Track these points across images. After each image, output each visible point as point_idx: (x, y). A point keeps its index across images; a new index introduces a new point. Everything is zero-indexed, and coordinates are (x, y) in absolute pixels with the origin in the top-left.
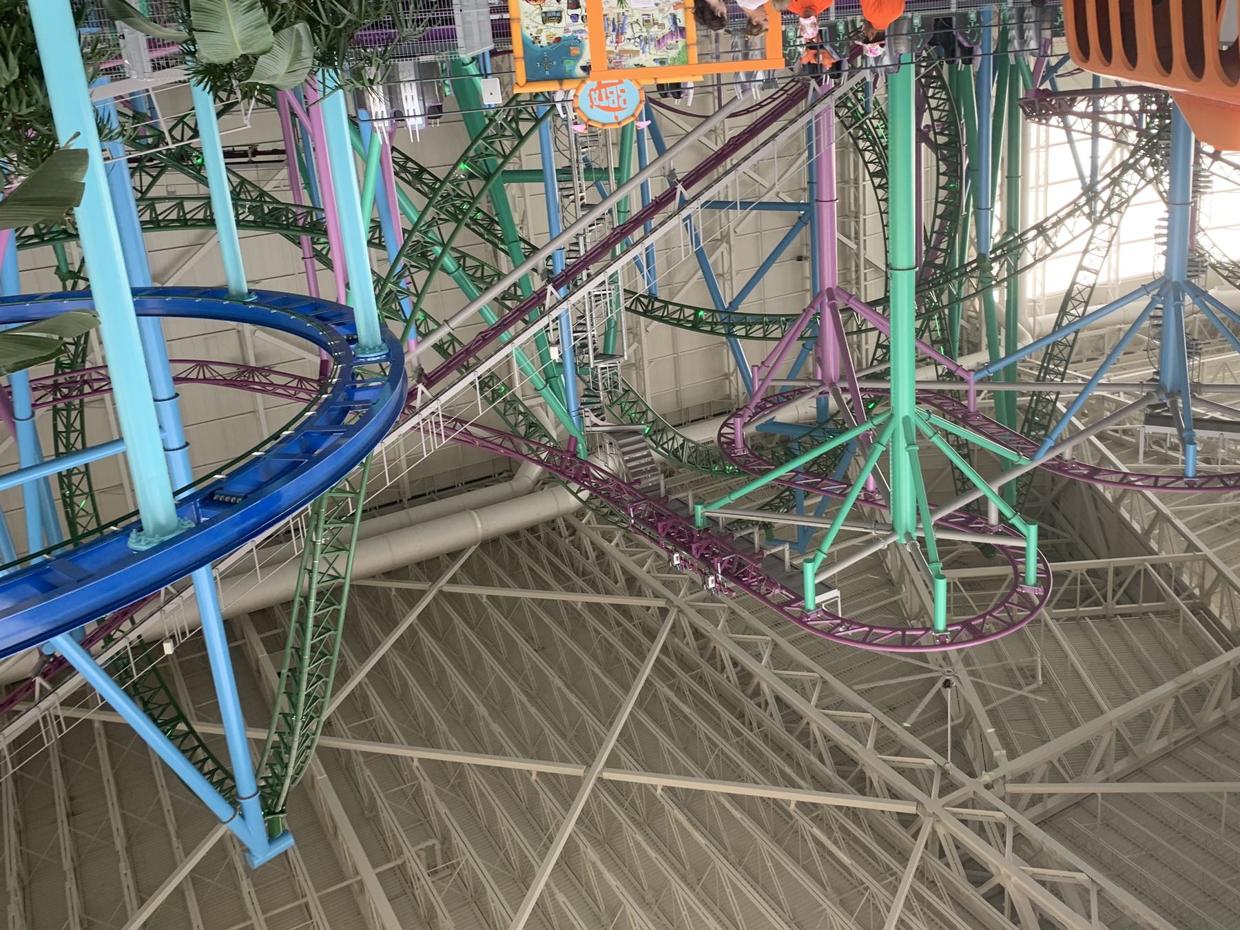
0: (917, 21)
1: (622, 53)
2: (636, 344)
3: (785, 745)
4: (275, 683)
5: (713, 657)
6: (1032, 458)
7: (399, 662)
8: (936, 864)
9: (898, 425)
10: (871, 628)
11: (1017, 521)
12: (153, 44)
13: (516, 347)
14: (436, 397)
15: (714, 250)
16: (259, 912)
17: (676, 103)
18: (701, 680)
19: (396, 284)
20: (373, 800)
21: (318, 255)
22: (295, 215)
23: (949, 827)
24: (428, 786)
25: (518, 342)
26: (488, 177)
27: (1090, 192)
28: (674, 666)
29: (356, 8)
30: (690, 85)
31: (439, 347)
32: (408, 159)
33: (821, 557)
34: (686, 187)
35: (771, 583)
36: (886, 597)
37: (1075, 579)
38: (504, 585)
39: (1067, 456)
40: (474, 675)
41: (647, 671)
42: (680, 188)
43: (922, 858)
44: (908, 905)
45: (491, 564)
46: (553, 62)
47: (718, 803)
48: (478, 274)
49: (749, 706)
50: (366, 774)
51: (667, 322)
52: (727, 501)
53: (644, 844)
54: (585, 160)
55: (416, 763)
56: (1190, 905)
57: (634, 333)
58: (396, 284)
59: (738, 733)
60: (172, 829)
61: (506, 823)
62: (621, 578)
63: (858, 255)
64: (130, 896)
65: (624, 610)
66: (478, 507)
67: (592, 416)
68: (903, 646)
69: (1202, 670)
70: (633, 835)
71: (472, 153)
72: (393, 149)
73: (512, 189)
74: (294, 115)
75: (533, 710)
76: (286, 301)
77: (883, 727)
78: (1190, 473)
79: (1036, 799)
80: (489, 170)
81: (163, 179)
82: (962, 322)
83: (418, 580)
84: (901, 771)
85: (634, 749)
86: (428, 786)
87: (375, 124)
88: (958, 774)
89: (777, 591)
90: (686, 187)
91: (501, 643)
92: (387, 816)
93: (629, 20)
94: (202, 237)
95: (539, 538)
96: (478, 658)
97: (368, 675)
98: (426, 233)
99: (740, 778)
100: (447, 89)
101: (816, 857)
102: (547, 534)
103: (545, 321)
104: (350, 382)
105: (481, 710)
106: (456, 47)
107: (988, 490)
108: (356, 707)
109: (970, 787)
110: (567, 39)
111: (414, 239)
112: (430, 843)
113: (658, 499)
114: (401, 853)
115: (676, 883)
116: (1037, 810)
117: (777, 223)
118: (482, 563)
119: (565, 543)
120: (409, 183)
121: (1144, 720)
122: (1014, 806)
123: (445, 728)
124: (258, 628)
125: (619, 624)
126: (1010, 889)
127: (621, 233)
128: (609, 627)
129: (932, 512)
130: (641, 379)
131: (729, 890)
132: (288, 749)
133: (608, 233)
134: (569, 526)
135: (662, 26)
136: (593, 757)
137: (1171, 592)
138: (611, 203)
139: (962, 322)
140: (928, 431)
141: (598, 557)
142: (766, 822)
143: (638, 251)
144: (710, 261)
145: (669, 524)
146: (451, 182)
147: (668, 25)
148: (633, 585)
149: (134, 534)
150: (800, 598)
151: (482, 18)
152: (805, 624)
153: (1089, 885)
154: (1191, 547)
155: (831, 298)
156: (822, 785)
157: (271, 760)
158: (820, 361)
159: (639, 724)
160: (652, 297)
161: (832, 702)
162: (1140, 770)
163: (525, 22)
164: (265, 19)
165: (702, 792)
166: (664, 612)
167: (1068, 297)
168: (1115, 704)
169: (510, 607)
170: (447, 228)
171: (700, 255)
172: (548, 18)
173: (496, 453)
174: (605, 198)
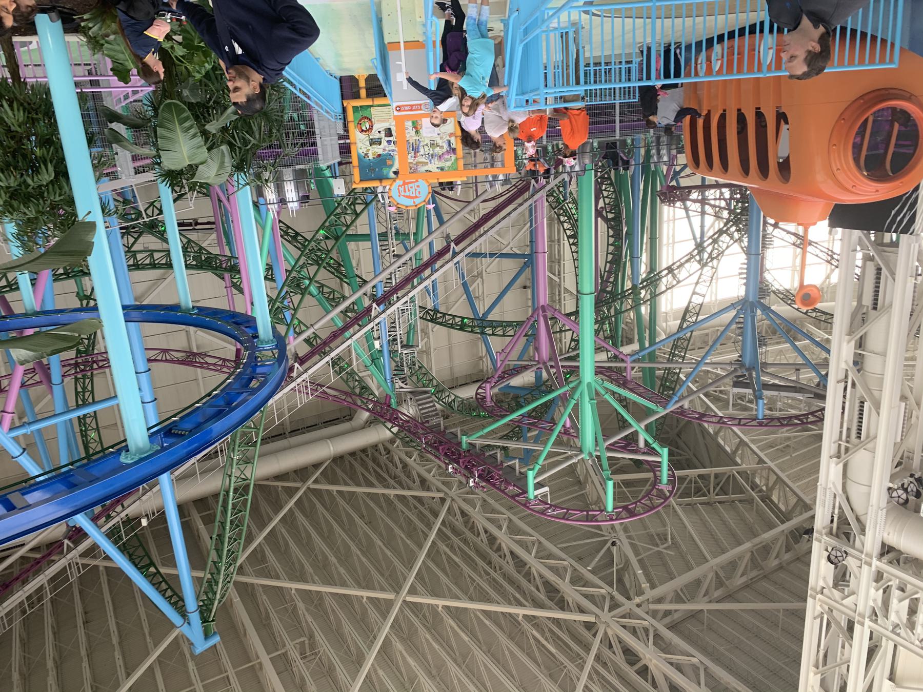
0: (595, 144)
1: (418, 163)
3: (516, 581)
4: (209, 543)
5: (473, 528)
6: (665, 408)
7: (283, 530)
8: (607, 652)
9: (584, 387)
10: (568, 510)
11: (655, 446)
12: (135, 158)
13: (354, 341)
14: (306, 371)
15: (473, 282)
17: (450, 194)
18: (465, 541)
19: (282, 302)
21: (235, 285)
23: (616, 630)
24: (301, 605)
25: (355, 338)
26: (337, 238)
27: (700, 247)
28: (449, 533)
29: (257, 136)
30: (459, 183)
31: (307, 341)
32: (289, 227)
33: (538, 467)
34: (456, 244)
35: (508, 483)
36: (576, 491)
37: (691, 480)
38: (346, 484)
40: (328, 538)
41: (433, 536)
42: (453, 245)
43: (599, 649)
44: (590, 677)
45: (338, 471)
47: (476, 615)
48: (331, 297)
49: (495, 557)
50: (263, 598)
51: (445, 326)
52: (481, 433)
53: (431, 640)
54: (395, 228)
55: (293, 591)
57: (425, 332)
58: (282, 302)
59: (487, 574)
60: (146, 631)
61: (348, 628)
62: (417, 480)
63: (560, 285)
64: (121, 672)
65: (419, 499)
66: (331, 437)
68: (587, 521)
69: (767, 536)
70: (424, 635)
71: (327, 224)
72: (280, 221)
73: (351, 246)
74: (220, 201)
75: (364, 559)
77: (575, 569)
79: (667, 613)
80: (337, 234)
81: (141, 240)
82: (623, 326)
83: (295, 481)
84: (586, 596)
85: (425, 583)
86: (301, 605)
87: (269, 206)
88: (620, 598)
89: (511, 488)
90: (456, 244)
91: (345, 519)
92: (277, 624)
93: (422, 144)
94: (164, 274)
95: (367, 456)
97: (265, 538)
98: (299, 272)
99: (489, 601)
101: (535, 648)
102: (373, 453)
105: (333, 559)
106: (317, 160)
107: (638, 427)
108: (257, 558)
109: (628, 606)
110: (385, 155)
112: (302, 639)
113: (439, 433)
114: (284, 646)
116: (668, 620)
117: (511, 267)
118: (333, 471)
119: (383, 459)
120: (289, 242)
121: (732, 565)
123: (311, 570)
125: (416, 508)
126: (651, 667)
127: (417, 272)
128: (410, 510)
129: (605, 440)
131: (482, 668)
132: (217, 583)
134: (386, 449)
136: (400, 588)
138: (411, 254)
139: (623, 326)
140: (602, 392)
141: (403, 468)
142: (506, 629)
143: (428, 283)
144: (471, 289)
147: (446, 146)
148: (424, 484)
149: (123, 454)
150: (525, 492)
151: (333, 142)
152: (528, 507)
153: (699, 665)
154: (761, 461)
155: (544, 311)
157: (206, 589)
158: (537, 349)
159: (428, 568)
160: (436, 311)
161: (544, 555)
162: (730, 595)
163: (359, 145)
164: (203, 143)
165: (466, 609)
166: (443, 500)
169: (350, 498)
170: (313, 269)
171: (465, 285)
172: (373, 142)
173: (343, 404)
174: (407, 251)
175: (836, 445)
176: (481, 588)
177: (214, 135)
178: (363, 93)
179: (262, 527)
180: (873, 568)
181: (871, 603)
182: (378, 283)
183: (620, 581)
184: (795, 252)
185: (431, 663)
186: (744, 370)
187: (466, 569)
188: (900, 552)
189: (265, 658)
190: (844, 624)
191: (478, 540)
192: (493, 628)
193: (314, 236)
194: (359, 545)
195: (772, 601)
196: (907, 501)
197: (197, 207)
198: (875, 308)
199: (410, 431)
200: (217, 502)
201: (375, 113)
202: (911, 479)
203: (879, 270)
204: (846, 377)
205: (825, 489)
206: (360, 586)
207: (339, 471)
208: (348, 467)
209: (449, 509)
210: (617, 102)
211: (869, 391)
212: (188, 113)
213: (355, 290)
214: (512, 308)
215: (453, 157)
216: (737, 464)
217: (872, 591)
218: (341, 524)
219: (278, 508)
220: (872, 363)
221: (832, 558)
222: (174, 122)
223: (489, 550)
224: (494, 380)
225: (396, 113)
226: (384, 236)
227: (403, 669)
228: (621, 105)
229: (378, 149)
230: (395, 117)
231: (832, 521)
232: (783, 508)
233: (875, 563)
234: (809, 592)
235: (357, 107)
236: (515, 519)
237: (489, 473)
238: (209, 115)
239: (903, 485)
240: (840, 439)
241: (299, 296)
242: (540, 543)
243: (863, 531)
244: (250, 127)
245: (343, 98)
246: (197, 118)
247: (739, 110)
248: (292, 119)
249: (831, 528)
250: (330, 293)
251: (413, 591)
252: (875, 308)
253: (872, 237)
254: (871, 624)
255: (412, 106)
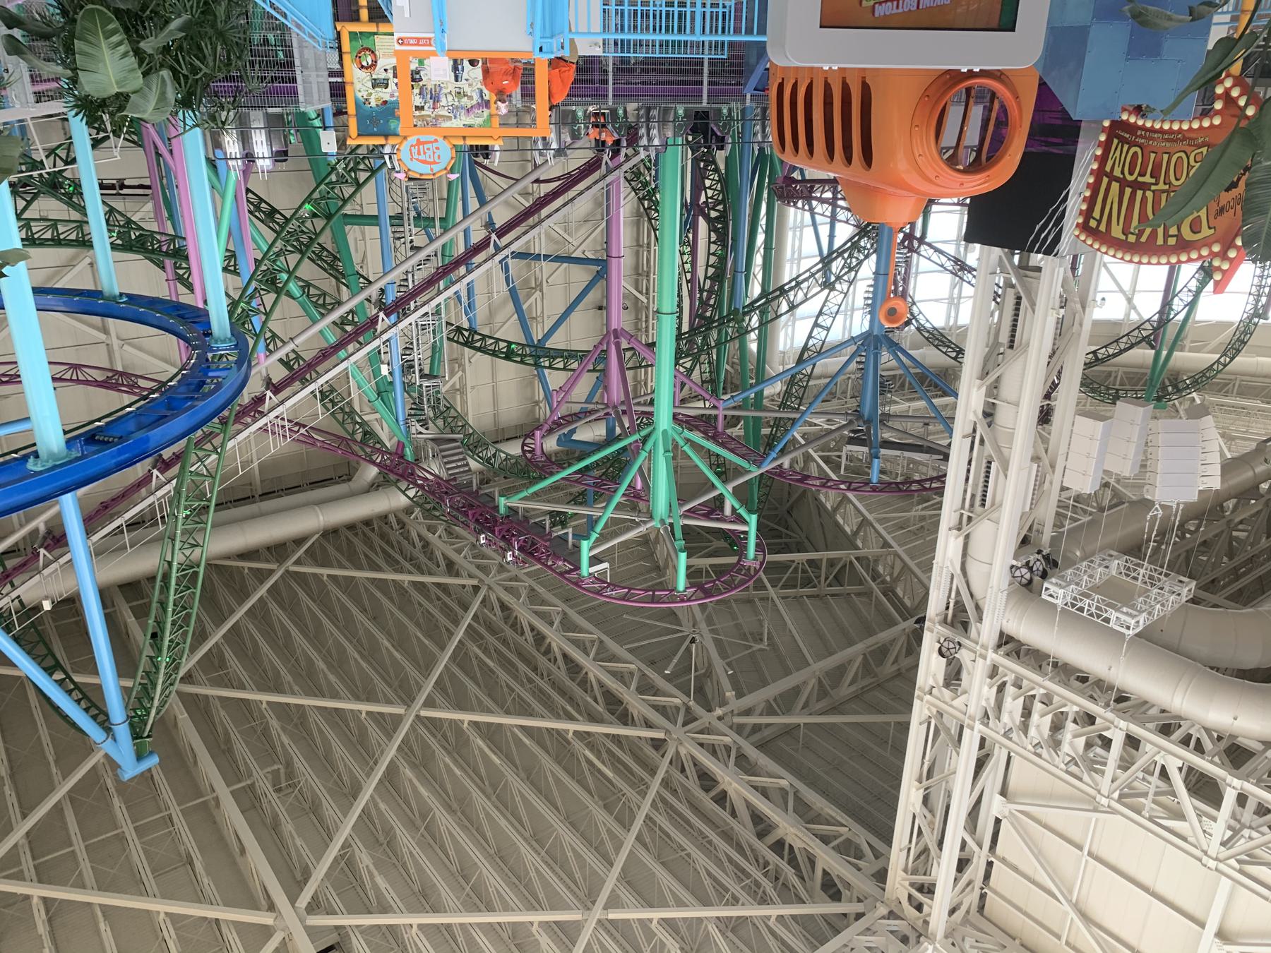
0: (681, 112)
1: (437, 118)
2: (460, 373)
3: (568, 689)
4: (140, 637)
5: (515, 625)
6: (759, 467)
7: (251, 627)
8: (677, 775)
9: (658, 436)
10: (630, 589)
11: (742, 512)
12: (34, 79)
13: (354, 359)
14: (282, 403)
15: (529, 296)
16: (129, 822)
17: (486, 162)
18: (504, 642)
19: (248, 303)
20: (227, 733)
21: (180, 279)
22: (159, 242)
23: (689, 749)
24: (274, 724)
25: (353, 359)
26: (329, 217)
27: (826, 261)
28: (482, 630)
29: (211, 64)
30: (497, 148)
31: (285, 363)
32: (261, 200)
33: (594, 536)
34: (499, 237)
35: (556, 557)
36: (654, 579)
37: (796, 569)
38: (342, 567)
39: (786, 466)
40: (316, 637)
41: (460, 634)
42: (494, 237)
43: (667, 772)
44: (654, 804)
45: (330, 549)
46: (380, 120)
47: (513, 734)
48: (321, 302)
49: (542, 661)
50: (222, 715)
51: (485, 352)
52: (524, 494)
53: (451, 765)
54: (415, 209)
55: (264, 705)
56: (862, 803)
57: (457, 362)
58: (248, 303)
59: (530, 681)
60: (51, 759)
61: (339, 750)
62: (442, 563)
63: (647, 308)
64: (14, 812)
65: (443, 588)
66: (321, 503)
67: (418, 426)
68: (652, 602)
69: (884, 636)
70: (444, 759)
71: (316, 195)
72: (248, 191)
73: (353, 233)
74: (158, 155)
75: (364, 665)
76: (152, 303)
77: (644, 675)
78: (875, 480)
79: (757, 728)
80: (329, 210)
81: (35, 204)
82: (728, 367)
83: (267, 561)
84: (656, 708)
85: (447, 694)
86: (274, 724)
87: (230, 162)
88: (698, 710)
89: (560, 563)
90: (499, 237)
91: (339, 613)
92: (241, 748)
93: (444, 91)
94: (74, 257)
95: (373, 530)
96: (319, 625)
97: (224, 636)
98: (274, 261)
99: (530, 714)
100: (292, 138)
101: (587, 773)
102: (380, 528)
103: (376, 343)
104: (204, 366)
105: (321, 665)
106: (297, 102)
107: (725, 490)
108: (213, 666)
109: (706, 718)
110: (392, 103)
111: (264, 268)
112: (276, 767)
113: (470, 493)
114: (250, 775)
115: (476, 795)
116: (757, 737)
117: (581, 276)
118: (324, 549)
119: (395, 535)
120: (262, 221)
121: (841, 670)
122: (739, 733)
123: (289, 678)
124: (127, 595)
125: (439, 599)
126: (731, 793)
127: (445, 271)
128: (431, 601)
129: (680, 505)
130: (464, 402)
131: (518, 799)
132: (154, 685)
133: (433, 271)
134: (399, 521)
135: (470, 98)
136: (413, 700)
137: (869, 579)
138: (437, 245)
139: (727, 366)
140: (681, 443)
141: (423, 547)
142: (551, 750)
143: (461, 287)
144: (525, 307)
145: (472, 507)
146: (297, 220)
147: (476, 98)
148: (451, 568)
149: (32, 459)
150: (578, 568)
151: (321, 80)
152: (580, 587)
153: (788, 789)
154: (886, 545)
155: (616, 337)
156: (593, 718)
157: (138, 702)
158: (606, 388)
159: (452, 676)
160: (472, 331)
161: (604, 655)
162: (834, 708)
163: (358, 86)
164: (136, 65)
165: (500, 725)
166: (476, 589)
167: (805, 348)
168: (819, 658)
169: (348, 585)
170: (293, 259)
171: (513, 293)
172: (376, 84)
173: (338, 454)
174: (431, 241)
175: (958, 514)
176: (522, 699)
177: (150, 55)
178: (364, 14)
179: (220, 621)
180: (988, 662)
181: (984, 703)
182: (390, 282)
183: (700, 691)
184: (952, 280)
185: (451, 794)
186: (861, 423)
187: (503, 676)
188: (1020, 643)
189: (224, 792)
190: (954, 731)
191: (520, 640)
192: (536, 749)
193: (294, 214)
194: (358, 646)
195: (881, 713)
196: (1030, 581)
197: (126, 161)
198: (1011, 347)
199: (436, 492)
200: (153, 588)
201: (380, 43)
202: (1039, 557)
203: (1019, 298)
204: (974, 431)
205: (942, 568)
206: (358, 698)
207: (331, 550)
208: (344, 543)
209: (483, 601)
210: (706, 57)
211: (998, 449)
212: (114, 25)
213: (355, 290)
214: (579, 333)
215: (486, 112)
216: (857, 548)
217: (986, 688)
218: (333, 619)
219: (243, 595)
220: (1004, 415)
221: (944, 650)
222: (97, 34)
223: (535, 653)
224: (546, 427)
225: (398, 47)
226: (397, 219)
227: (413, 803)
228: (712, 62)
229: (384, 94)
230: (397, 53)
231: (947, 608)
232: (908, 602)
233: (992, 656)
234: (917, 693)
235: (355, 33)
236: (572, 614)
237: (533, 544)
238: (145, 28)
239: (1028, 563)
240: (963, 508)
241: (273, 296)
242: (601, 642)
243: (980, 619)
244: (200, 49)
245: (337, 18)
246: (127, 30)
247: (826, 82)
248: (266, 42)
249: (946, 615)
250: (319, 296)
251: (430, 703)
252: (1011, 347)
253: (1016, 259)
254: (981, 727)
255: (418, 39)
